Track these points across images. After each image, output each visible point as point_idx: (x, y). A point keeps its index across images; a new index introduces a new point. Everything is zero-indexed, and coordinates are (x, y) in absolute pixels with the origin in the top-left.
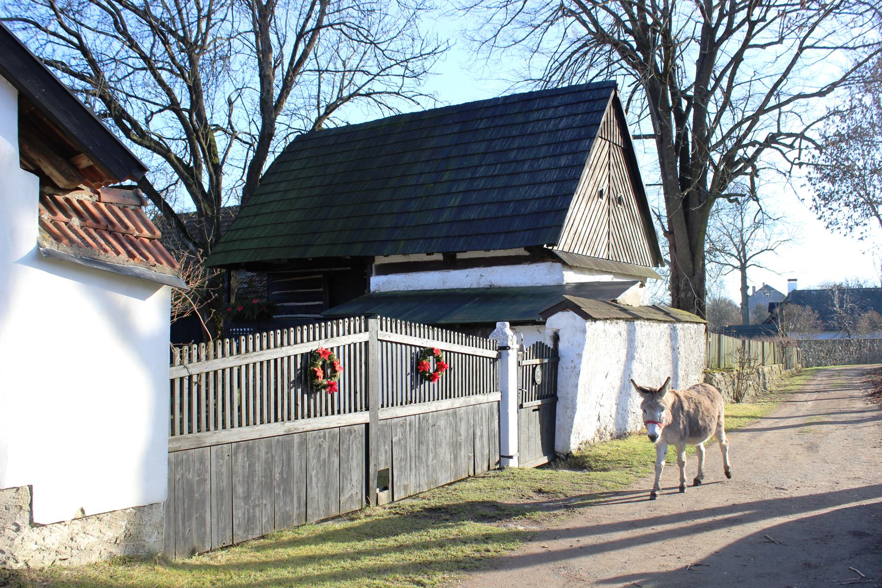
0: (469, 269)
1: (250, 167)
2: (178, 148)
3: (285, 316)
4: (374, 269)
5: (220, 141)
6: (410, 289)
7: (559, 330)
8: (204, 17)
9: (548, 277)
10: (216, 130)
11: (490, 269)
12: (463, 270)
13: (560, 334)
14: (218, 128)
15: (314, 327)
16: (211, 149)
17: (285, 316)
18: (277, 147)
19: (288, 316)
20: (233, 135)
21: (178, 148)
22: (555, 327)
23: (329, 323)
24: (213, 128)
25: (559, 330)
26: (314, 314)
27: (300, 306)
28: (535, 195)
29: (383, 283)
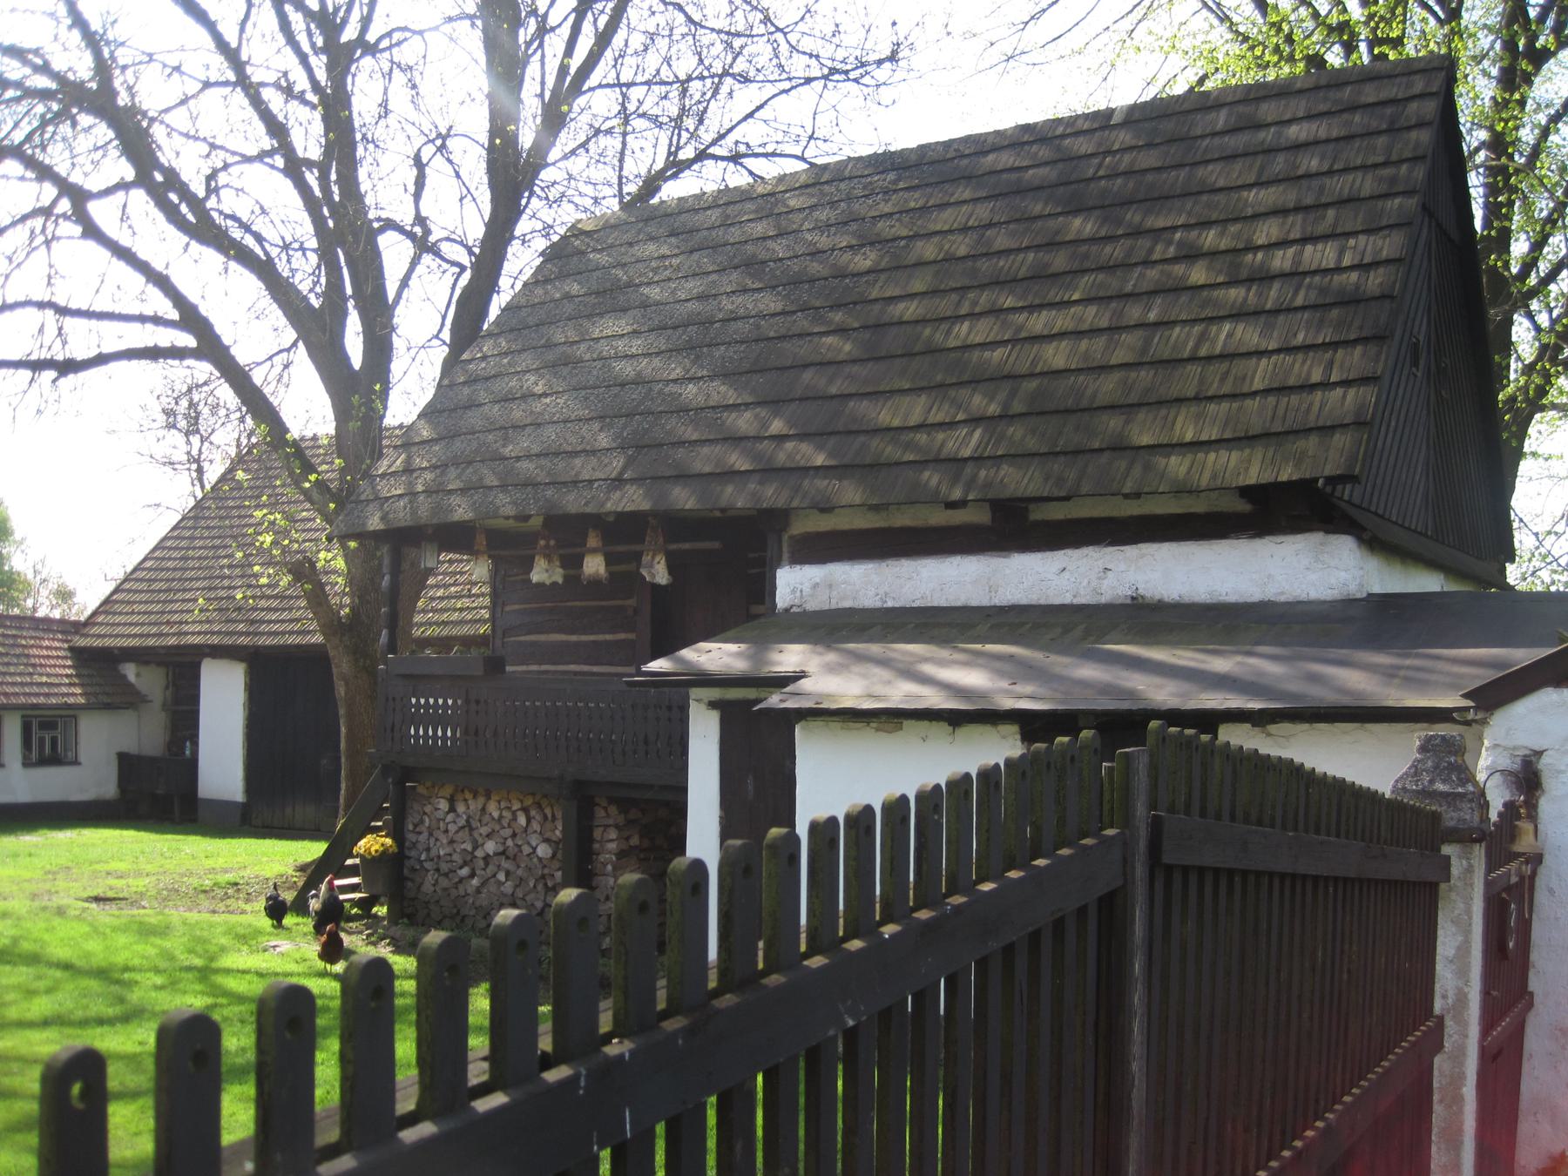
0: (1069, 552)
1: (458, 302)
2: (304, 273)
3: (534, 668)
4: (785, 549)
5: (394, 252)
6: (890, 604)
7: (1539, 754)
8: (1059, 149)
9: (1313, 577)
10: (382, 230)
11: (1131, 551)
12: (1048, 554)
13: (1544, 763)
14: (390, 225)
15: (69, 667)
16: (368, 267)
17: (534, 668)
18: (521, 262)
19: (544, 667)
20: (423, 245)
21: (304, 273)
22: (1527, 740)
23: (69, 663)
24: (376, 225)
25: (1539, 754)
26: (611, 664)
27: (577, 644)
28: (1197, 346)
29: (816, 586)
